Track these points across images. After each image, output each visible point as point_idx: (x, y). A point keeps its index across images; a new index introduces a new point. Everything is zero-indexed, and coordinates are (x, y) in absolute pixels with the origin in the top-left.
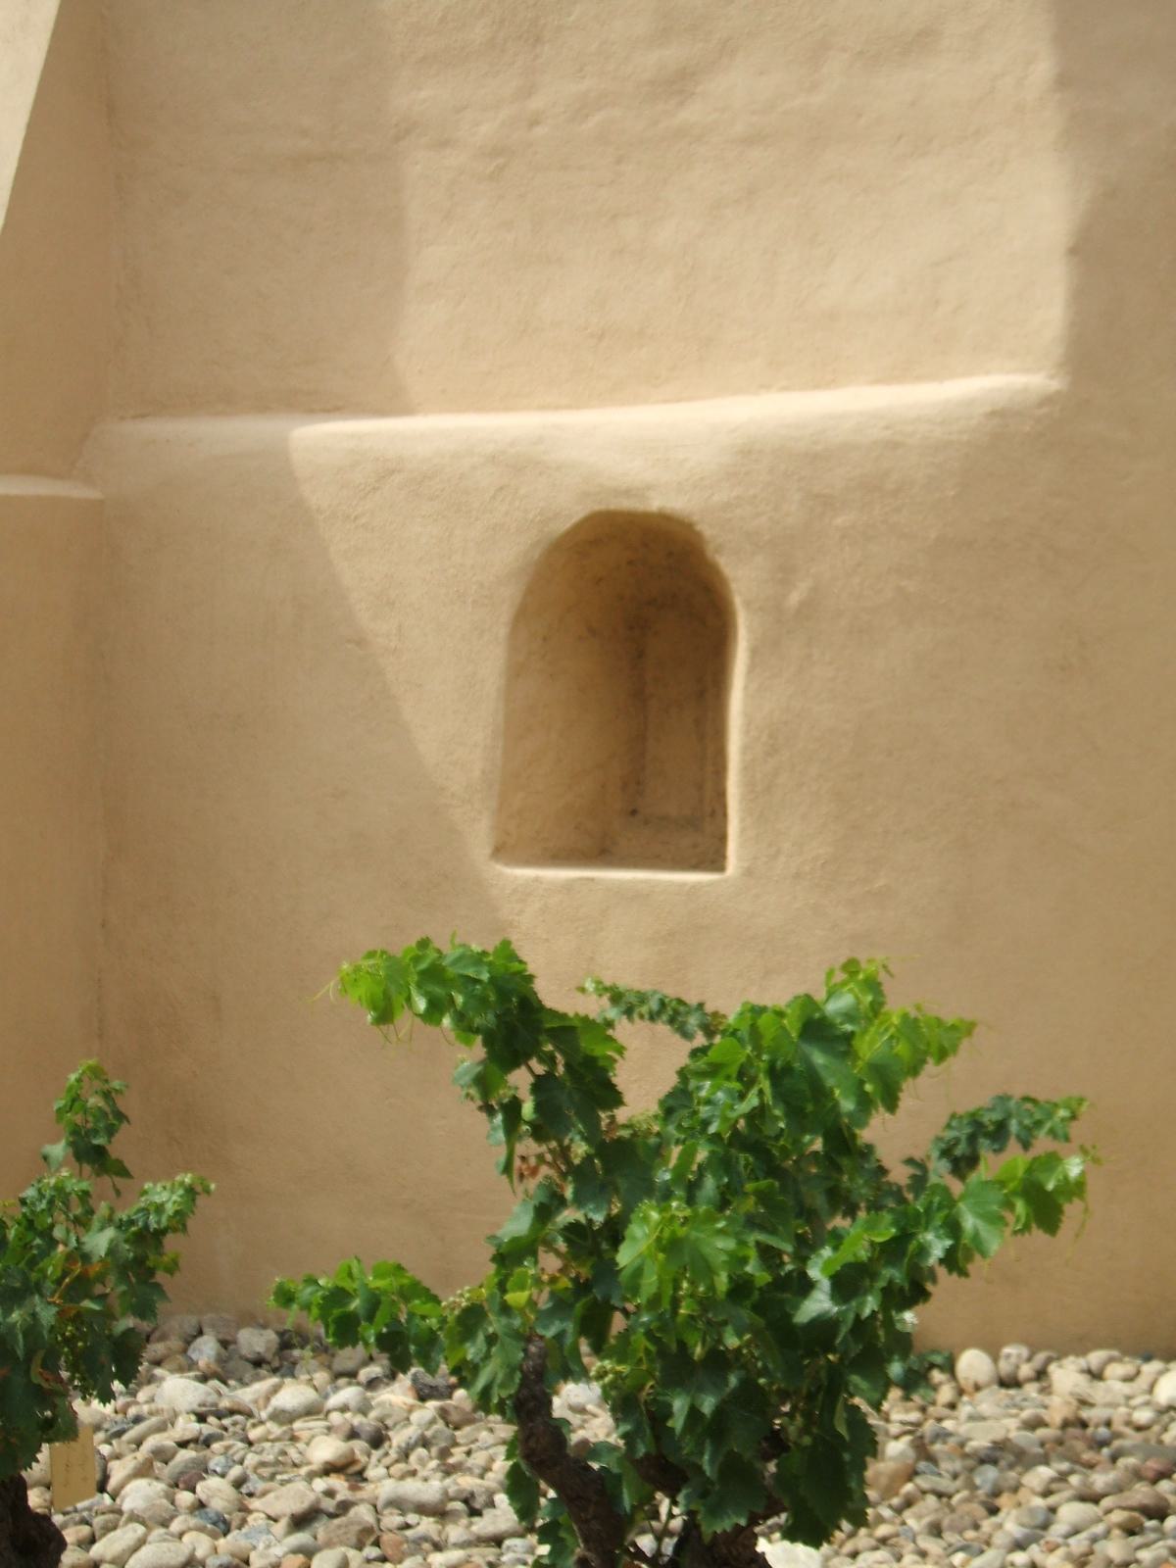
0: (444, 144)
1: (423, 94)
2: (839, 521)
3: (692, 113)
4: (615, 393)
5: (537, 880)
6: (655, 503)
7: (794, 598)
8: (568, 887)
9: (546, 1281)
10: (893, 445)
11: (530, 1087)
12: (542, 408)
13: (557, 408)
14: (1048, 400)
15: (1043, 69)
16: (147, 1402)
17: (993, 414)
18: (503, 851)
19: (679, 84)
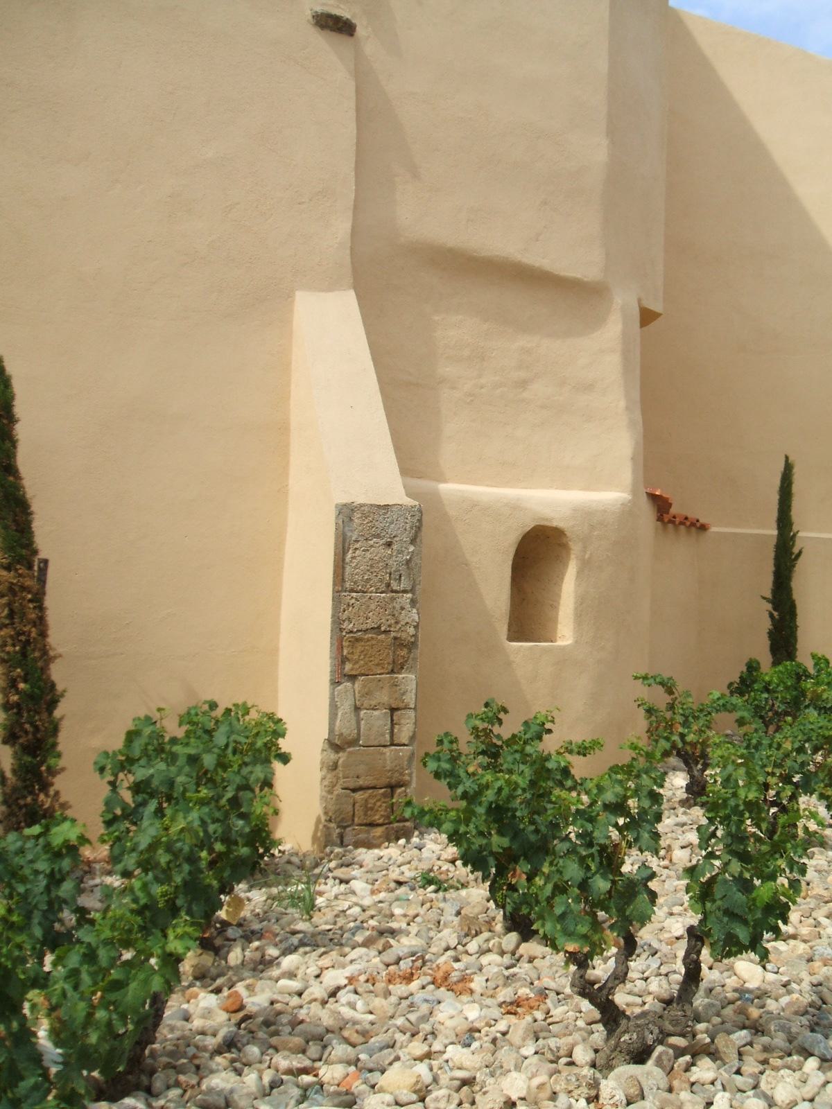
0: (453, 388)
1: (448, 369)
2: (595, 533)
3: (525, 395)
4: (506, 484)
5: (521, 646)
6: (555, 524)
7: (587, 556)
8: (531, 648)
9: (204, 755)
10: (605, 511)
11: (60, 687)
12: (487, 486)
13: (492, 486)
14: (630, 501)
15: (622, 404)
16: (721, 899)
17: (622, 504)
18: (511, 639)
19: (523, 384)
